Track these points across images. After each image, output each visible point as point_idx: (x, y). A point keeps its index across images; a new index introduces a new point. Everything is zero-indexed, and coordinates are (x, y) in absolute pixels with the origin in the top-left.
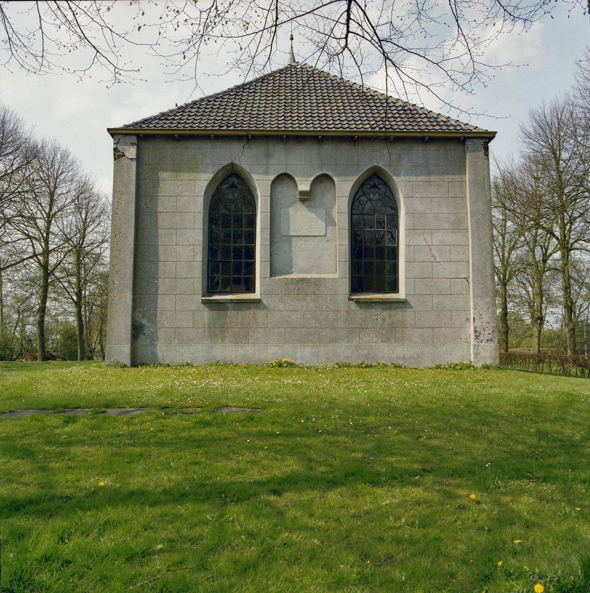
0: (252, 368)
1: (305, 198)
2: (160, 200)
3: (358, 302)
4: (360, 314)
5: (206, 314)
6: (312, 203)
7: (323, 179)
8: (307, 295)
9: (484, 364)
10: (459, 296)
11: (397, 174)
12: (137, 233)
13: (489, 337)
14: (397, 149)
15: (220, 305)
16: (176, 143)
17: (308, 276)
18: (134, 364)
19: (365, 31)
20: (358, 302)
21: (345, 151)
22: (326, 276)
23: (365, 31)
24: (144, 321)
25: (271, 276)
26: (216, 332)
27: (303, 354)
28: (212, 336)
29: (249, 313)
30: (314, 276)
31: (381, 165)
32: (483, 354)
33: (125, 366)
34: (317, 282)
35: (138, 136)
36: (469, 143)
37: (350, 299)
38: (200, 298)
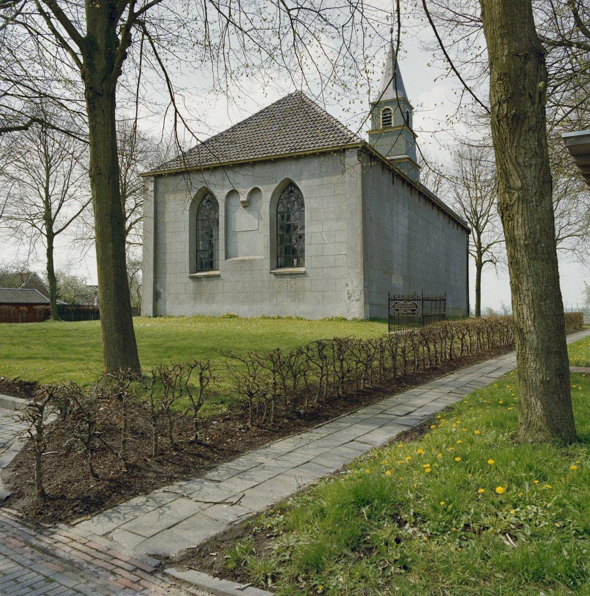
0: (213, 318)
1: (246, 205)
2: (167, 215)
3: (275, 274)
4: (278, 282)
5: (191, 285)
6: (251, 208)
7: (256, 190)
8: (246, 271)
9: (353, 317)
10: (341, 268)
11: (300, 180)
12: (420, 193)
13: (358, 298)
14: (301, 164)
15: (283, 275)
16: (175, 177)
17: (247, 258)
18: (155, 315)
19: (180, 116)
20: (275, 274)
21: (268, 169)
22: (257, 257)
23: (180, 116)
24: (161, 290)
25: (226, 259)
26: (197, 296)
27: (243, 310)
28: (195, 298)
29: (213, 283)
30: (251, 258)
31: (290, 177)
32: (353, 310)
33: (150, 317)
34: (251, 262)
35: (154, 176)
36: (347, 153)
37: (271, 273)
38: (188, 274)
